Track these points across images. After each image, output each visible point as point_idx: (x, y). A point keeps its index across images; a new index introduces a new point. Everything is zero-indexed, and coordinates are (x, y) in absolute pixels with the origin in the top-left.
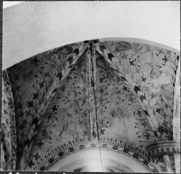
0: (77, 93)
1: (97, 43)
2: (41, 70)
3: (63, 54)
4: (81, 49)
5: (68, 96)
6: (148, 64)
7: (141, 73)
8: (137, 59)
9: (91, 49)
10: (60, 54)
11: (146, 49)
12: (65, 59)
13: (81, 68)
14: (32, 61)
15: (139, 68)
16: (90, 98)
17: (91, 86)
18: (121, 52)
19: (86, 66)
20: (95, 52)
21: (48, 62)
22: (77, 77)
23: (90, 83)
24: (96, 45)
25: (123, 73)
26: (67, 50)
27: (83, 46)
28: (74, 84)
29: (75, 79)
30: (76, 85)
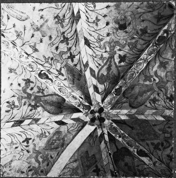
0: (35, 31)
1: (89, 120)
2: (107, 18)
3: (103, 67)
4: (97, 98)
5: (42, 13)
6: (12, 161)
7: (6, 147)
8: (27, 148)
9: (85, 107)
10: (105, 61)
11: (33, 167)
12: (95, 62)
13: (65, 69)
14: (127, 23)
15: (15, 146)
16: (135, 153)
17: (42, 71)
18: (52, 135)
19: (65, 79)
20: (81, 110)
21: (108, 39)
22: (55, 51)
23: (47, 73)
24: (87, 117)
25: (28, 127)
26: (103, 75)
27: (99, 103)
28: (50, 37)
29: (56, 45)
30: (46, 39)
